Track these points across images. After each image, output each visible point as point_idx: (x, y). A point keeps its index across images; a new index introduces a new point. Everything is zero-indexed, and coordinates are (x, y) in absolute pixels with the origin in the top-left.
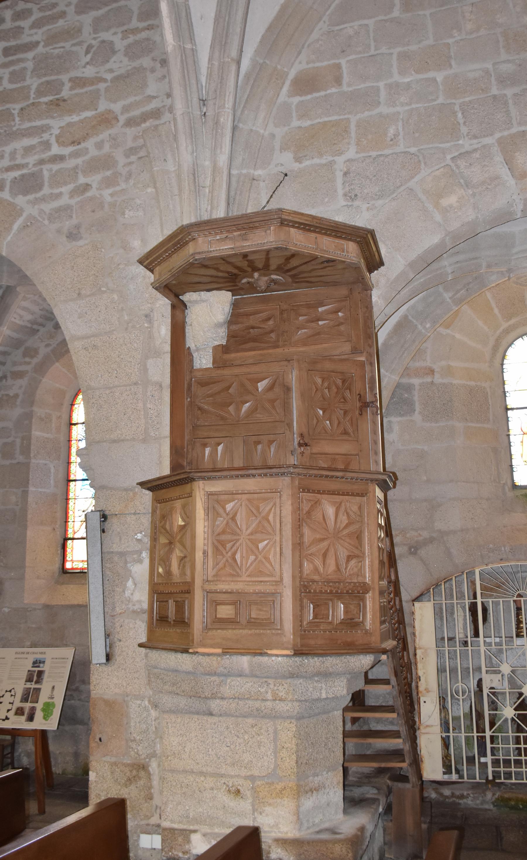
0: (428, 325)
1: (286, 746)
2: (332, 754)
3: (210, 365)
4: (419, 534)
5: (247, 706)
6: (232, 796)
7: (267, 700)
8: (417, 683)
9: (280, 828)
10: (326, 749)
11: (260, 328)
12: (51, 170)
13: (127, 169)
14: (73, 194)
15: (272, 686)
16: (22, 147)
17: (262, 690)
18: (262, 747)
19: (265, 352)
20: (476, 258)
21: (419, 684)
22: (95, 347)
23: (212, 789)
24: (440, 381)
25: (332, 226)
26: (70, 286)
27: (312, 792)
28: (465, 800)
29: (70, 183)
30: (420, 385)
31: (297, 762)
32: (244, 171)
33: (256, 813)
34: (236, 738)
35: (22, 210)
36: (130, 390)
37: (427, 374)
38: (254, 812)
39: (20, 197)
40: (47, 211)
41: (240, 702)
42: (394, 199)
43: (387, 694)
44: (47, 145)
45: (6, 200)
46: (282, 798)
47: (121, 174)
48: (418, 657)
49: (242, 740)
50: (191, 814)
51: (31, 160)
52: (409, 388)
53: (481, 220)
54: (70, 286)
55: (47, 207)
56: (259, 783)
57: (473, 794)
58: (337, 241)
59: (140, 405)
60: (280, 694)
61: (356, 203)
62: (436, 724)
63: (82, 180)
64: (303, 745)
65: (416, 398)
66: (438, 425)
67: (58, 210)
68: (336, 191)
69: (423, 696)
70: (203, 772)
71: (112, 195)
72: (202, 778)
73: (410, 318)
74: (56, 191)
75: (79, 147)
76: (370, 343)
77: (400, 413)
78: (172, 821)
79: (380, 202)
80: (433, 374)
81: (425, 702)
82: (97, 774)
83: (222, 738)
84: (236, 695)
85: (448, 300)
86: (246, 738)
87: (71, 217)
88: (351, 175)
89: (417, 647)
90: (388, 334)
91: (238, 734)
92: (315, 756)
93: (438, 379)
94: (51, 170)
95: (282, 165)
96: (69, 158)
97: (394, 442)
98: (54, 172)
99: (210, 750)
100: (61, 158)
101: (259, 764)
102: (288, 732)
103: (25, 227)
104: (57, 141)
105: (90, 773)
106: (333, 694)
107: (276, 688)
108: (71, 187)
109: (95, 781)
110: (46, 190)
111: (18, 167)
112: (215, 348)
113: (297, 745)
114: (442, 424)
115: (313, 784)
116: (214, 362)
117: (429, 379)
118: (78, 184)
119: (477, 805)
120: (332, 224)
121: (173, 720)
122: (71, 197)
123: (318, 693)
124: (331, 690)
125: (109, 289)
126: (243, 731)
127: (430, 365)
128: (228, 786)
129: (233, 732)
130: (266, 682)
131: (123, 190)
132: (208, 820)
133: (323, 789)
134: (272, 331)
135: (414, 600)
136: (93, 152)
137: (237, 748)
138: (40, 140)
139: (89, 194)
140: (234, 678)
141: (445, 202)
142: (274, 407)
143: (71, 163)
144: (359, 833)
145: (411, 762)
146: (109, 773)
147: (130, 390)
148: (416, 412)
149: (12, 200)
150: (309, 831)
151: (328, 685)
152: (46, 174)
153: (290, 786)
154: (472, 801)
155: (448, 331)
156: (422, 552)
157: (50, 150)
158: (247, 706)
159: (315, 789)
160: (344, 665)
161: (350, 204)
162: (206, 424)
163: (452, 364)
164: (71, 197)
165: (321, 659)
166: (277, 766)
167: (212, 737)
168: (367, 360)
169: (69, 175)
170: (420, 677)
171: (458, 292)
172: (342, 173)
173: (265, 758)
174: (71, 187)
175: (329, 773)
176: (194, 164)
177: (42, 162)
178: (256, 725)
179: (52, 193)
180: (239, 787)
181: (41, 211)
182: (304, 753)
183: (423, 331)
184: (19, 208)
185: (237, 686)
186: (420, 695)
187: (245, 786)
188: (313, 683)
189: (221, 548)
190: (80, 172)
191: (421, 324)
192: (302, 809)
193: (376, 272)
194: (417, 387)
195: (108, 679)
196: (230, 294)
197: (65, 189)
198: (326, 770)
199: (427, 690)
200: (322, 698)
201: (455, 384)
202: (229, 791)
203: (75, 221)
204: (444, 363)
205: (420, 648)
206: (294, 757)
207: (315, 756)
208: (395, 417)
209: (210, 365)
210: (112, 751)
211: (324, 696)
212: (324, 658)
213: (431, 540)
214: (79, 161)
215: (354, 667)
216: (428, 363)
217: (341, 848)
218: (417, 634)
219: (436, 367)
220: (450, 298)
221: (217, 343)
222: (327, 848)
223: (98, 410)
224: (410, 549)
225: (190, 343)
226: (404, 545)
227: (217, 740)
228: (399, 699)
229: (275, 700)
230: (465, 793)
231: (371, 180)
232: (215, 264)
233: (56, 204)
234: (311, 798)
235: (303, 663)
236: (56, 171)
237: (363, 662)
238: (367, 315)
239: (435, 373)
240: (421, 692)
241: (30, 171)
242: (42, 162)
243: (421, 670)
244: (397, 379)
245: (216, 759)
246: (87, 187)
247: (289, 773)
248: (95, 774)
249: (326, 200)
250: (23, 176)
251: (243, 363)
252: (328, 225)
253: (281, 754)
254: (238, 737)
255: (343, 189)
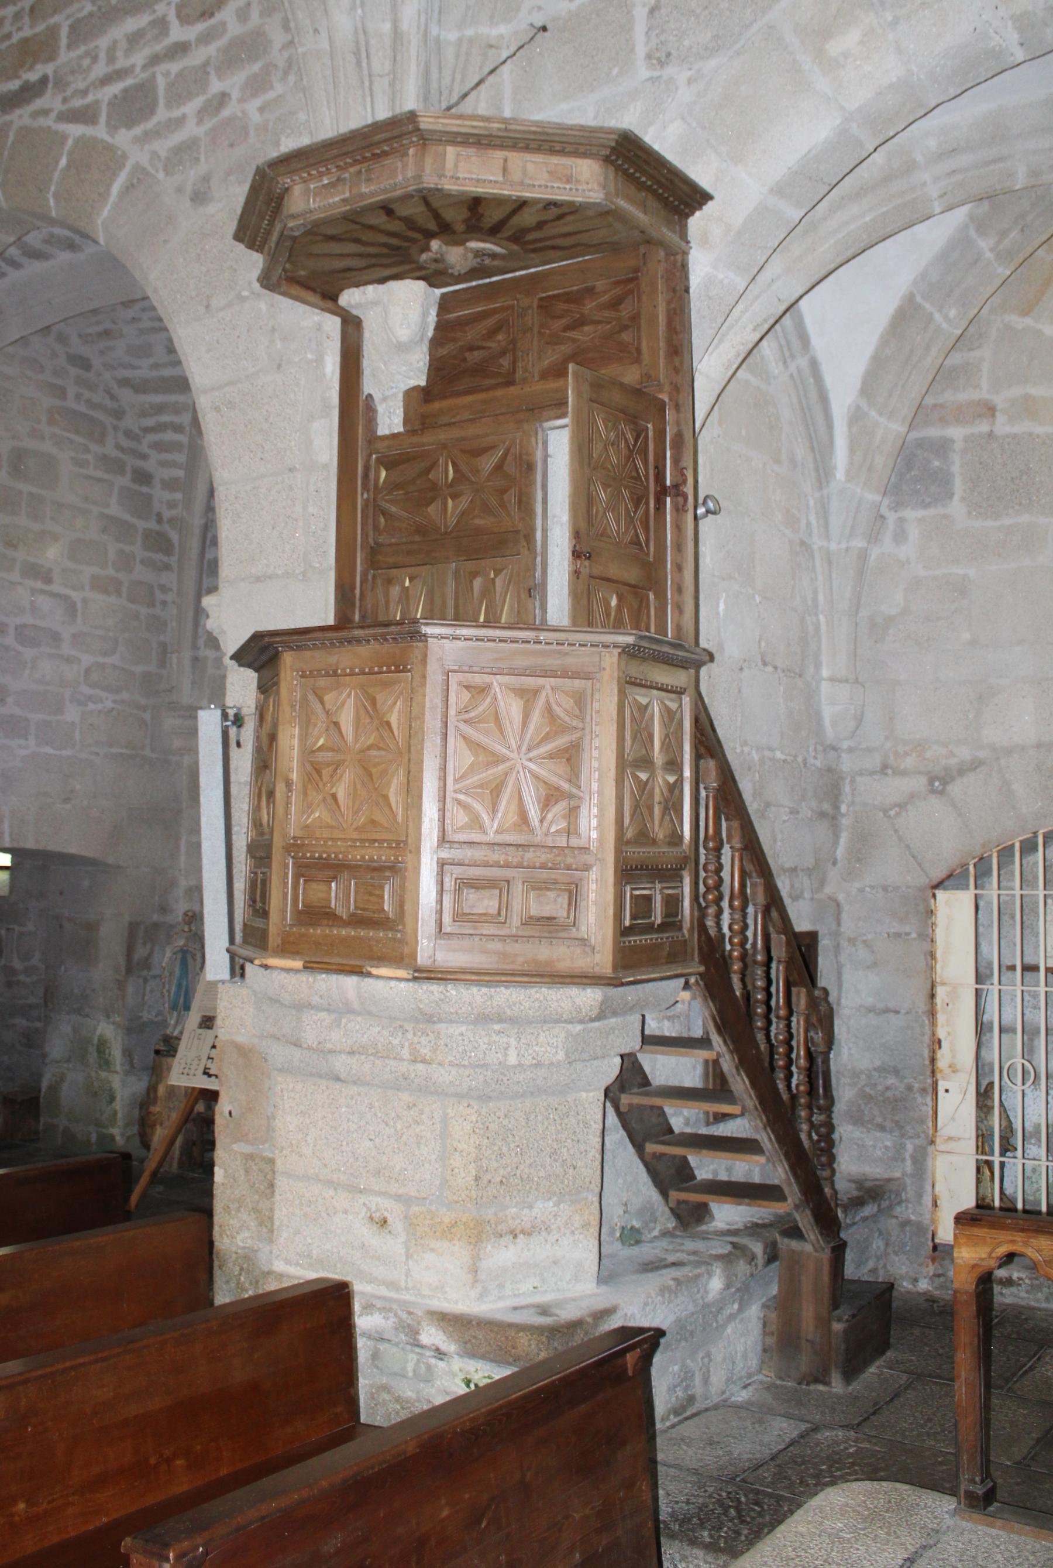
0: (953, 313)
1: (460, 1147)
2: (571, 1171)
3: (400, 429)
4: (951, 752)
5: (388, 1069)
6: (375, 1228)
7: (402, 1060)
8: (934, 1052)
9: (446, 1292)
10: (556, 1161)
11: (483, 348)
12: (167, 74)
13: (286, 54)
14: (202, 114)
15: (410, 1036)
16: (126, 35)
17: (396, 1042)
18: (422, 1146)
19: (491, 394)
20: (1001, 159)
21: (939, 1054)
22: (231, 405)
23: (346, 1212)
24: (1008, 429)
25: (535, 133)
26: (194, 294)
27: (515, 1237)
28: (1014, 1289)
29: (197, 95)
30: (966, 440)
31: (477, 1178)
32: (469, 32)
33: (410, 1262)
34: (383, 1125)
35: (125, 157)
36: (283, 482)
37: (980, 416)
38: (407, 1259)
39: (123, 130)
40: (163, 154)
41: (377, 1061)
42: (738, 53)
43: (875, 1069)
44: (161, 25)
45: (102, 141)
46: (450, 1241)
47: (276, 66)
48: (938, 1000)
49: (392, 1130)
50: (314, 1252)
51: (139, 58)
52: (942, 447)
53: (922, 76)
54: (194, 294)
55: (162, 146)
56: (415, 1209)
57: (1030, 1279)
58: (555, 160)
59: (299, 509)
60: (423, 1051)
61: (670, 71)
62: (967, 1135)
63: (216, 86)
64: (496, 1148)
65: (956, 468)
66: (998, 523)
67: (179, 150)
68: (632, 50)
69: (944, 1079)
70: (333, 1182)
71: (261, 110)
72: (332, 1192)
73: (919, 299)
74: (176, 113)
75: (212, 21)
76: (677, 364)
77: (923, 501)
78: (288, 1262)
79: (713, 63)
80: (993, 415)
81: (947, 1091)
82: (226, 1171)
83: (362, 1123)
84: (355, 1048)
85: (989, 255)
86: (399, 1127)
87: (197, 159)
88: (663, 11)
89: (938, 980)
90: (882, 337)
91: (386, 1119)
92: (526, 1170)
93: (1002, 426)
94: (167, 74)
95: (540, 8)
96: (197, 46)
97: (908, 562)
98: (173, 76)
99: (344, 1143)
100: (181, 49)
101: (417, 1176)
102: (465, 1123)
103: (129, 188)
104: (178, 16)
105: (216, 1169)
106: (533, 1058)
107: (416, 1040)
108: (198, 102)
109: (223, 1184)
110: (162, 113)
111: (120, 74)
112: (409, 394)
113: (479, 1147)
114: (1007, 521)
115: (518, 1221)
116: (406, 421)
117: (984, 427)
118: (209, 96)
119: (1038, 1301)
120: (533, 129)
121: (291, 1086)
122: (200, 122)
123: (499, 1055)
124: (530, 1052)
125: (253, 293)
126: (393, 1114)
127: (988, 397)
128: (369, 1209)
129: (379, 1115)
130: (401, 1026)
131: (279, 96)
132: (339, 1265)
133: (544, 1233)
134: (503, 353)
135: (936, 886)
136: (234, 29)
137: (385, 1143)
138: (151, 18)
139: (226, 113)
140: (352, 1017)
141: (834, 47)
142: (503, 505)
143: (197, 57)
144: (590, 1320)
145: (797, 1202)
146: (242, 1172)
147: (283, 482)
148: (956, 497)
149: (109, 139)
150: (501, 1304)
151: (523, 1041)
152: (161, 82)
153: (464, 1220)
154: (1027, 1292)
155: (1028, 321)
156: (955, 789)
157: (167, 34)
158: (388, 1069)
159: (523, 1232)
160: (537, 1004)
161: (656, 74)
162: (393, 540)
163: (1034, 391)
164: (200, 122)
165: (484, 990)
166: (445, 1182)
167: (348, 1121)
168: (670, 400)
169: (196, 81)
170: (940, 1041)
171: (1004, 234)
172: (646, 10)
173: (427, 1165)
174: (198, 102)
175: (562, 1206)
176: (356, 32)
177: (155, 60)
178: (415, 1105)
179: (170, 119)
180: (386, 1214)
181: (154, 154)
182: (495, 1165)
183: (944, 325)
184: (119, 153)
185: (357, 1031)
186: (939, 1076)
187: (393, 1211)
188: (490, 1036)
189: (315, 776)
190: (213, 72)
191: (940, 311)
192: (484, 1265)
193: (698, 214)
194: (958, 446)
195: (242, 1009)
196: (421, 284)
197: (190, 108)
198: (555, 1199)
199: (954, 1069)
200: (508, 1063)
201: (1038, 436)
202: (371, 1218)
203: (203, 168)
204: (1016, 391)
205: (943, 984)
206: (472, 1168)
207: (526, 1170)
208: (913, 509)
209: (400, 429)
210: (246, 1135)
211: (513, 1060)
212: (493, 990)
213: (975, 765)
214: (211, 50)
215: (559, 1010)
216: (982, 393)
217: (530, 1340)
218: (939, 955)
219: (999, 400)
220: (991, 250)
221: (413, 383)
222: (507, 1338)
223: (234, 522)
224: (931, 782)
225: (368, 386)
226: (920, 773)
227: (355, 1127)
228: (738, 1078)
229: (414, 1061)
230: (1015, 1275)
231: (697, 17)
232: (347, 232)
233: (176, 138)
234: (511, 1247)
235: (446, 997)
236: (176, 76)
237: (578, 1001)
238: (673, 306)
239: (998, 414)
240: (941, 1071)
241: (137, 81)
242: (155, 60)
243: (942, 1026)
244: (903, 429)
245: (351, 1160)
246: (223, 98)
247: (464, 1196)
248: (222, 1171)
249: (615, 71)
250: (126, 91)
251: (453, 420)
252: (524, 132)
253: (452, 1161)
254: (387, 1124)
255: (647, 43)
